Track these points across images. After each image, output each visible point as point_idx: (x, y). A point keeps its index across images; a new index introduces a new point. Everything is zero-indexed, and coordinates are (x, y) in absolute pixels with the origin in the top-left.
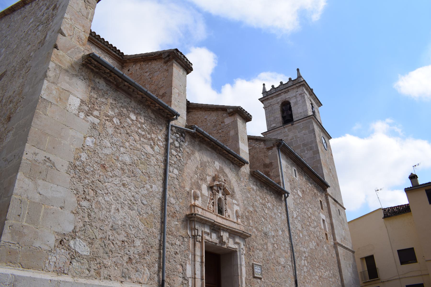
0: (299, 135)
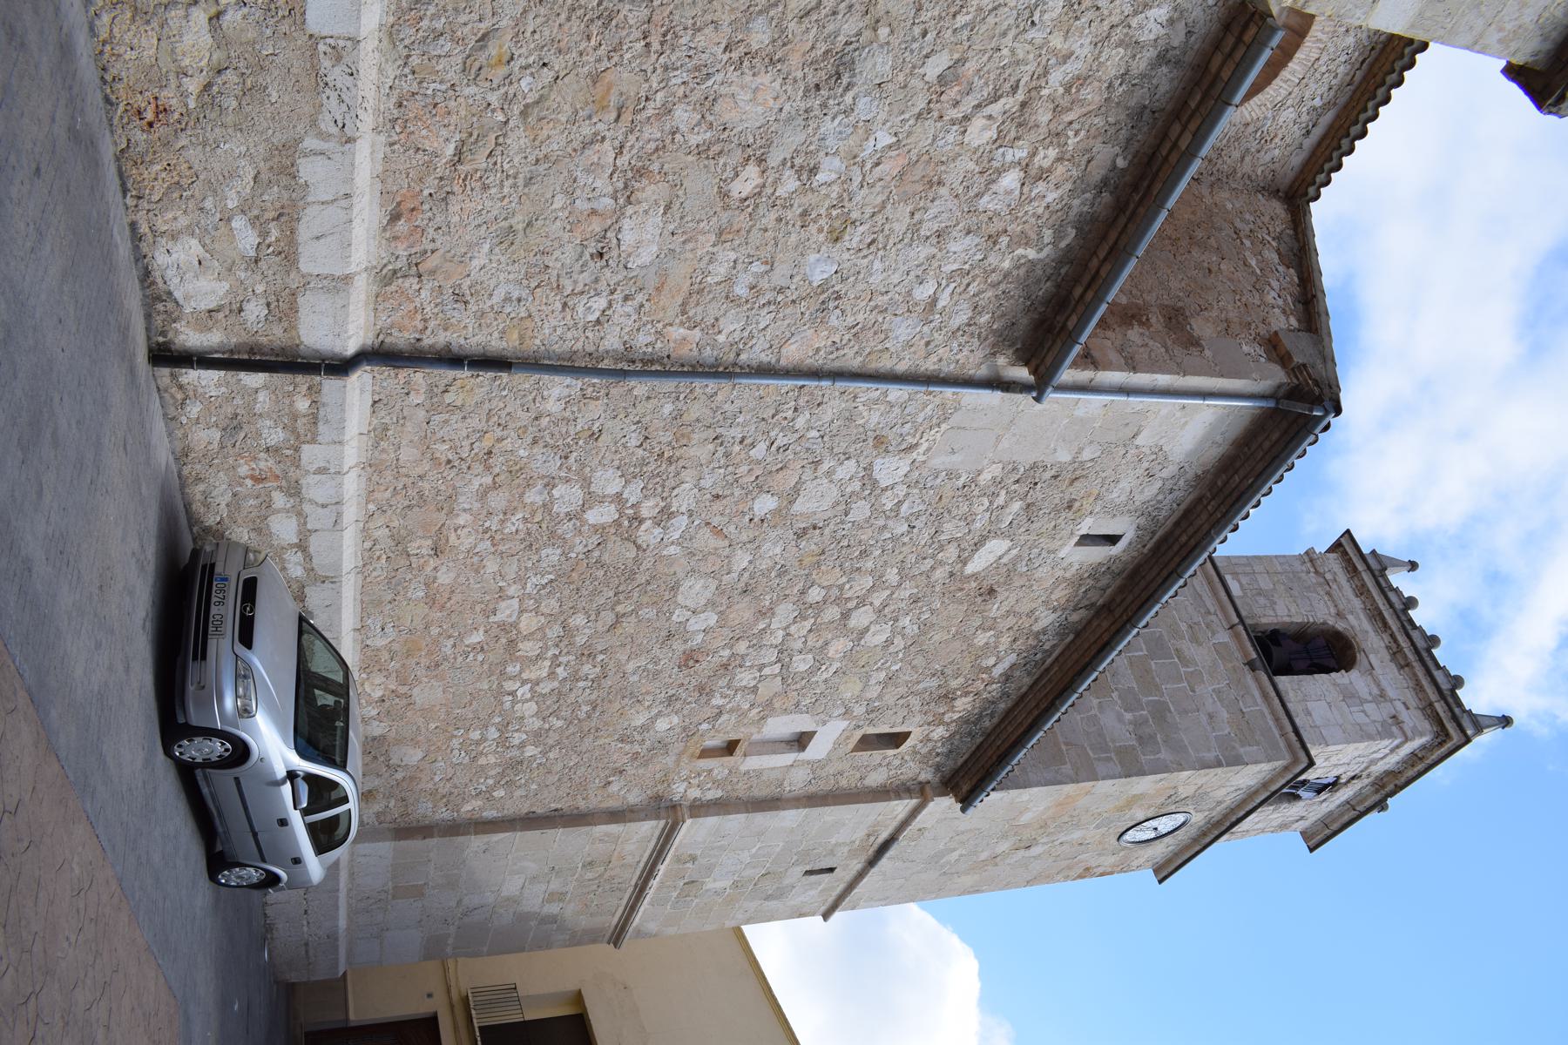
0: (1206, 689)
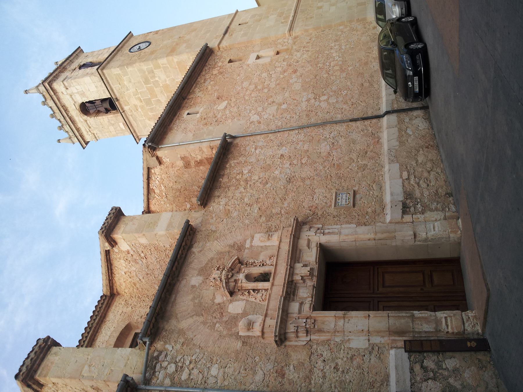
0: (132, 90)
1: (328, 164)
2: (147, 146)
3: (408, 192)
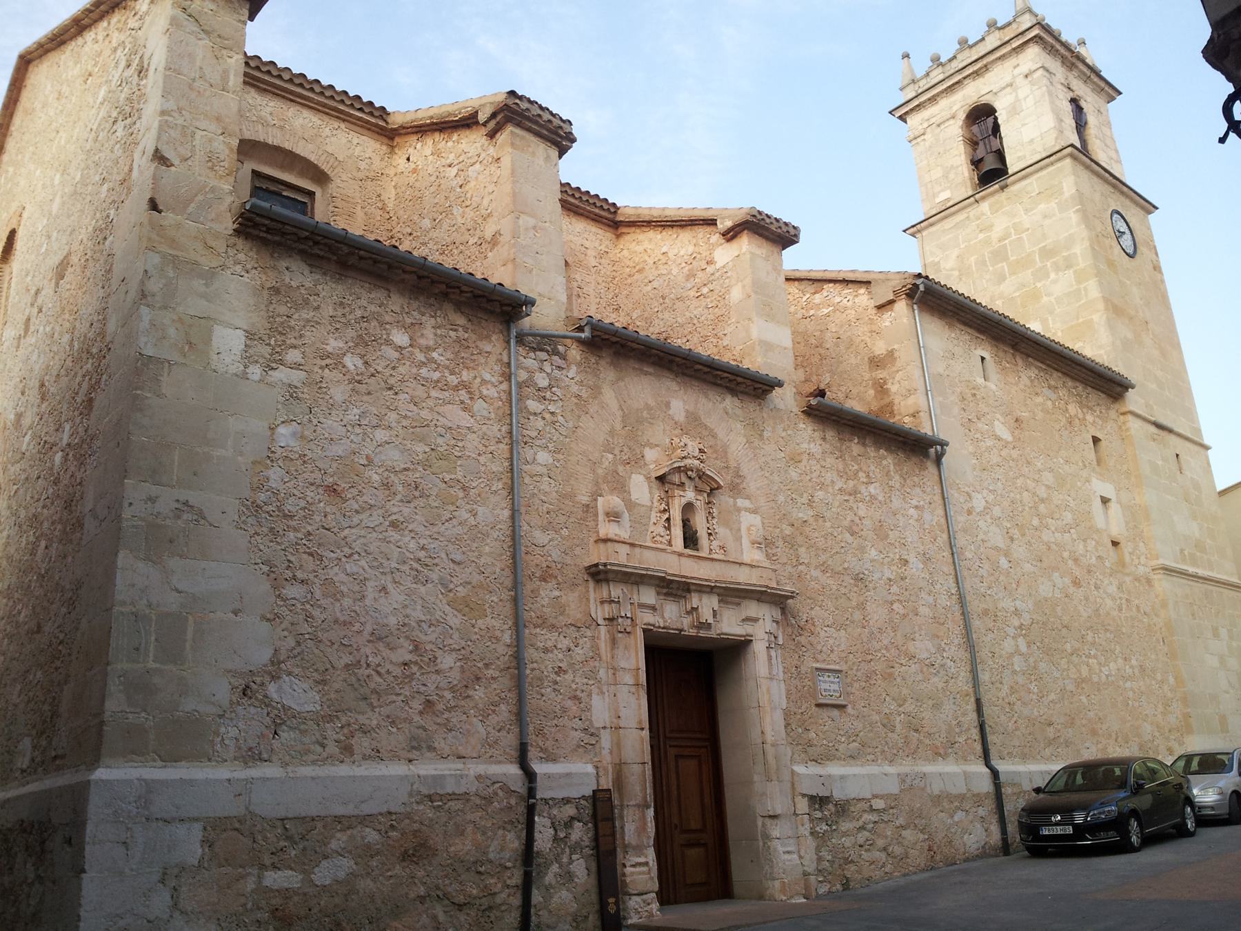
1: (893, 655)
2: (919, 282)
3: (848, 809)
